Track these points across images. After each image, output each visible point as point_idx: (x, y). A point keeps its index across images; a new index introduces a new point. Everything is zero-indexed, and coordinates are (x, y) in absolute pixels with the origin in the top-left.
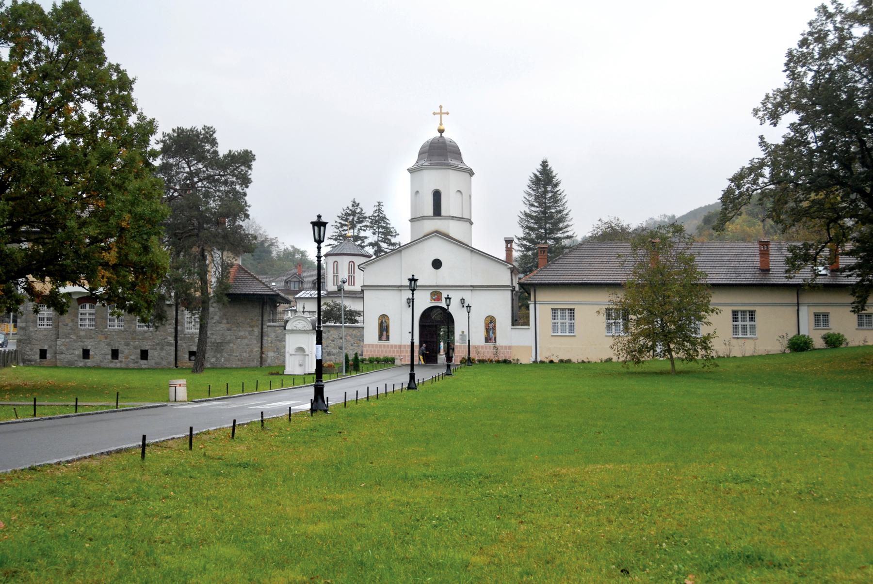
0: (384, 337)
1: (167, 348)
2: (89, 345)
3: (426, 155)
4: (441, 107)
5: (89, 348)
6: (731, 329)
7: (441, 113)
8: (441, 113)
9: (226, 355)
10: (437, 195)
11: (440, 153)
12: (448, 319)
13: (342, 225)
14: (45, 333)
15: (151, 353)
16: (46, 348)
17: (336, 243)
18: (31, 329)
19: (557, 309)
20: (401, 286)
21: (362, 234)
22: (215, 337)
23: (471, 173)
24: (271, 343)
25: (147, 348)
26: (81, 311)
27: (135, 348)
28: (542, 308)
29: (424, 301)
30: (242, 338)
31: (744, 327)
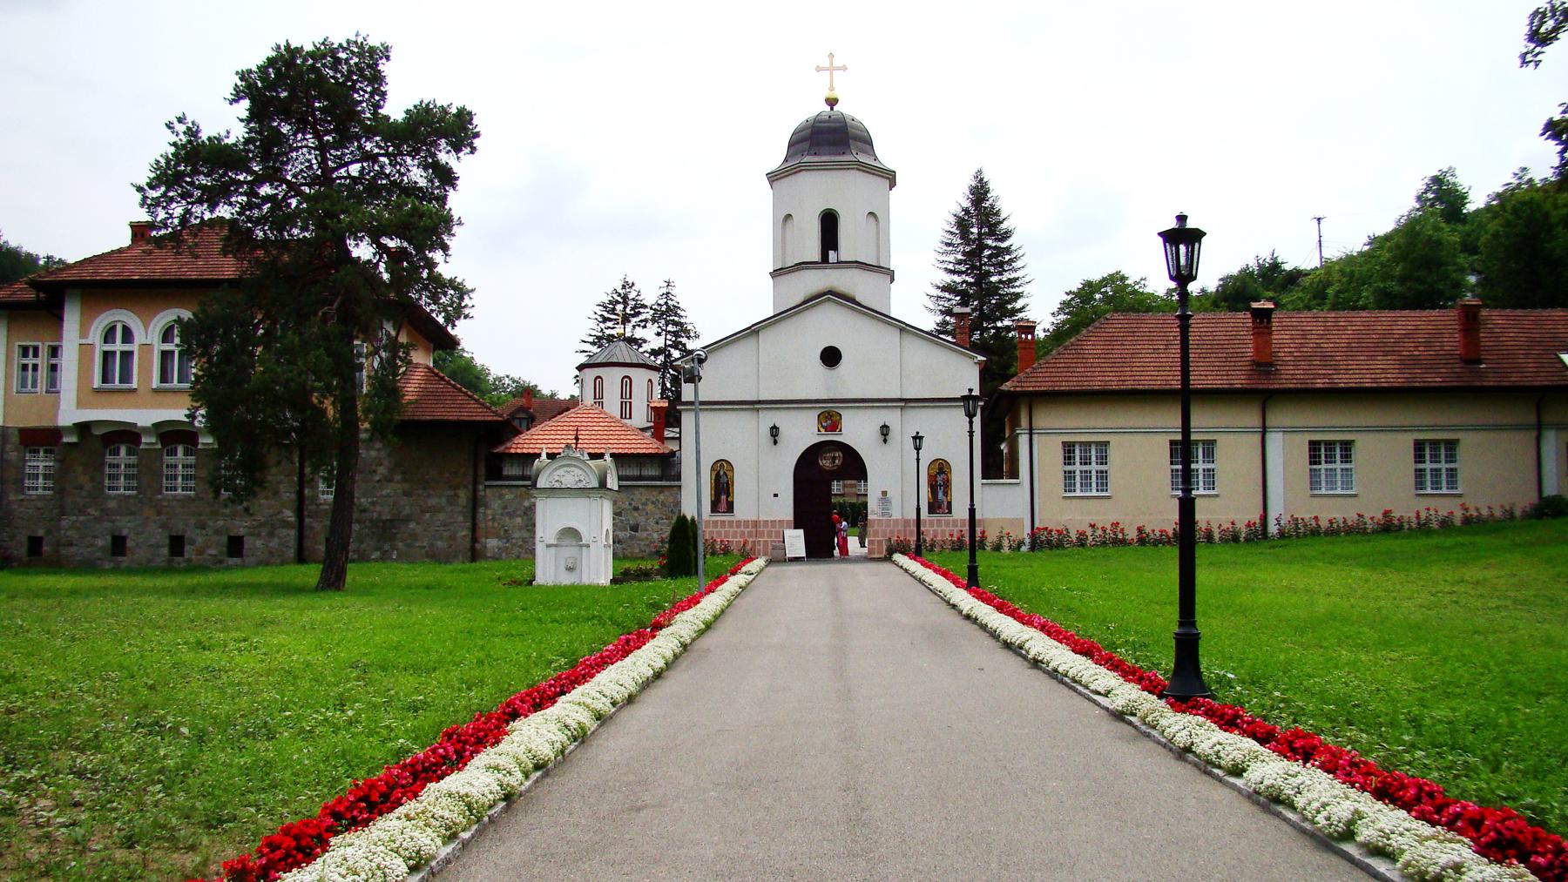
0: (723, 505)
1: (284, 532)
2: (126, 525)
3: (806, 145)
4: (831, 56)
5: (125, 532)
6: (1412, 479)
7: (832, 69)
9: (400, 545)
10: (829, 222)
11: (829, 141)
12: (853, 466)
13: (605, 320)
14: (39, 504)
15: (249, 542)
16: (41, 533)
17: (595, 349)
18: (12, 497)
19: (1089, 444)
20: (759, 402)
21: (639, 333)
22: (378, 508)
23: (890, 177)
24: (494, 519)
25: (242, 531)
26: (109, 459)
27: (218, 532)
28: (1041, 447)
29: (803, 432)
30: (435, 510)
31: (1086, 476)
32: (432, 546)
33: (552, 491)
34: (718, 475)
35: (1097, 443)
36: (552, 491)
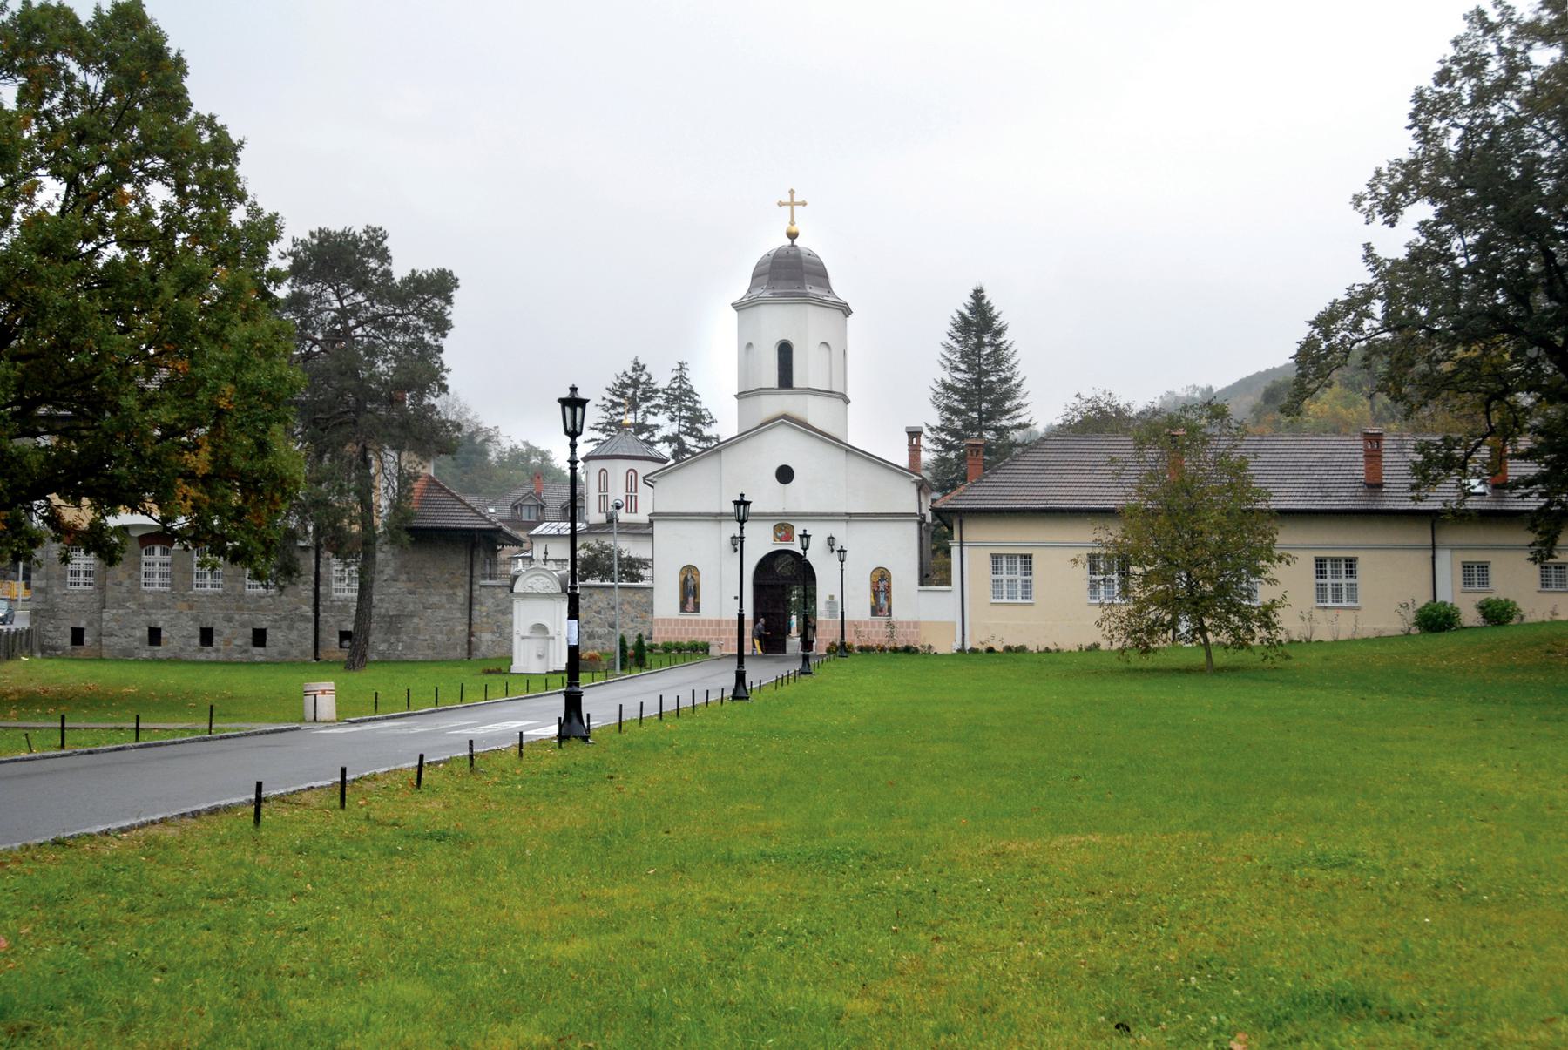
0: (690, 606)
1: (302, 625)
2: (161, 619)
4: (792, 192)
5: (160, 625)
7: (792, 204)
8: (792, 204)
10: (785, 350)
11: (791, 275)
12: (805, 574)
16: (82, 624)
17: (603, 436)
18: (56, 592)
20: (721, 514)
21: (651, 420)
23: (846, 311)
24: (488, 616)
25: (264, 625)
26: (145, 558)
27: (243, 625)
28: (974, 553)
29: (761, 542)
30: (434, 607)
32: (433, 638)
33: (525, 595)
34: (686, 579)
35: (1008, 556)
36: (525, 595)
